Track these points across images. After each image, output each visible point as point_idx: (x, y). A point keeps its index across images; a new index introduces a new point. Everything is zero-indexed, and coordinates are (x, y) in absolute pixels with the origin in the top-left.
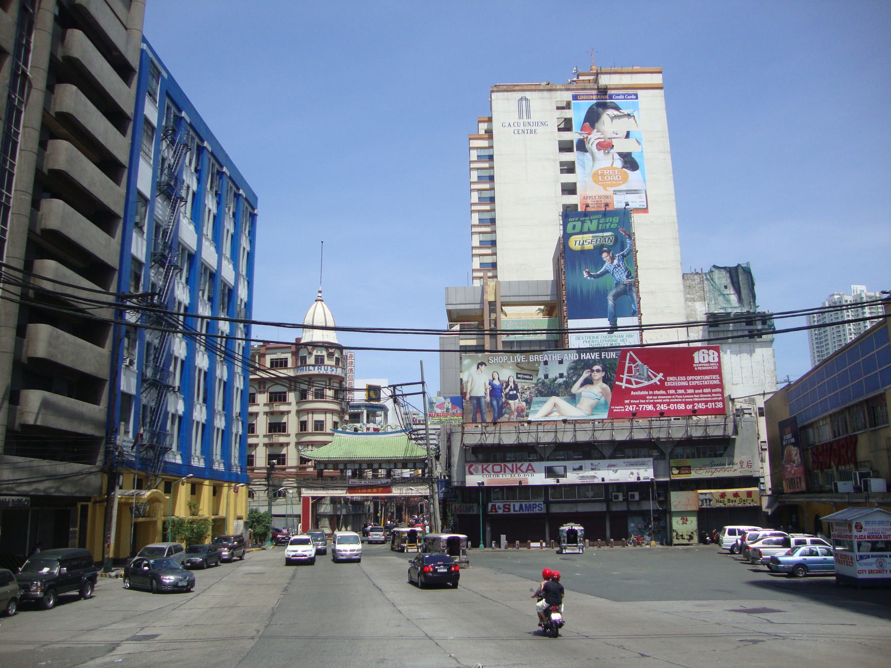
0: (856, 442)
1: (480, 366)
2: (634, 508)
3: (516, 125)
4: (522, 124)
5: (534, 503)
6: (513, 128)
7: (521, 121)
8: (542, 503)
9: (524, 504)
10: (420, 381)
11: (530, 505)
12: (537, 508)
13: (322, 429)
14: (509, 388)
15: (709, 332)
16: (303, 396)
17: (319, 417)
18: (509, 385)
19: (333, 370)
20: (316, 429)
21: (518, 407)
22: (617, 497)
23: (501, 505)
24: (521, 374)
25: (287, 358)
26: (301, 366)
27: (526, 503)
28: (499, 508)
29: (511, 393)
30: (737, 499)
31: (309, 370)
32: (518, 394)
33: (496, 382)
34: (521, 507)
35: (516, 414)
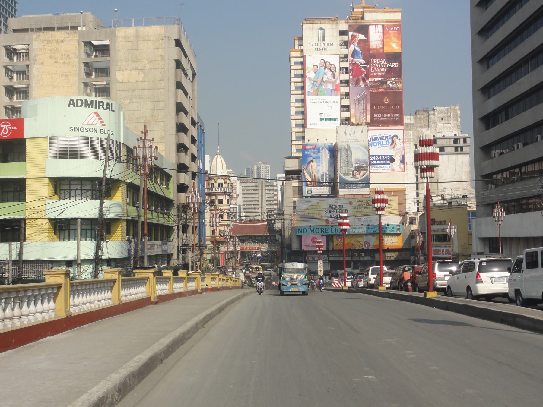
2: (361, 259)
3: (316, 45)
4: (320, 45)
6: (315, 47)
7: (320, 42)
23: (311, 257)
28: (310, 258)
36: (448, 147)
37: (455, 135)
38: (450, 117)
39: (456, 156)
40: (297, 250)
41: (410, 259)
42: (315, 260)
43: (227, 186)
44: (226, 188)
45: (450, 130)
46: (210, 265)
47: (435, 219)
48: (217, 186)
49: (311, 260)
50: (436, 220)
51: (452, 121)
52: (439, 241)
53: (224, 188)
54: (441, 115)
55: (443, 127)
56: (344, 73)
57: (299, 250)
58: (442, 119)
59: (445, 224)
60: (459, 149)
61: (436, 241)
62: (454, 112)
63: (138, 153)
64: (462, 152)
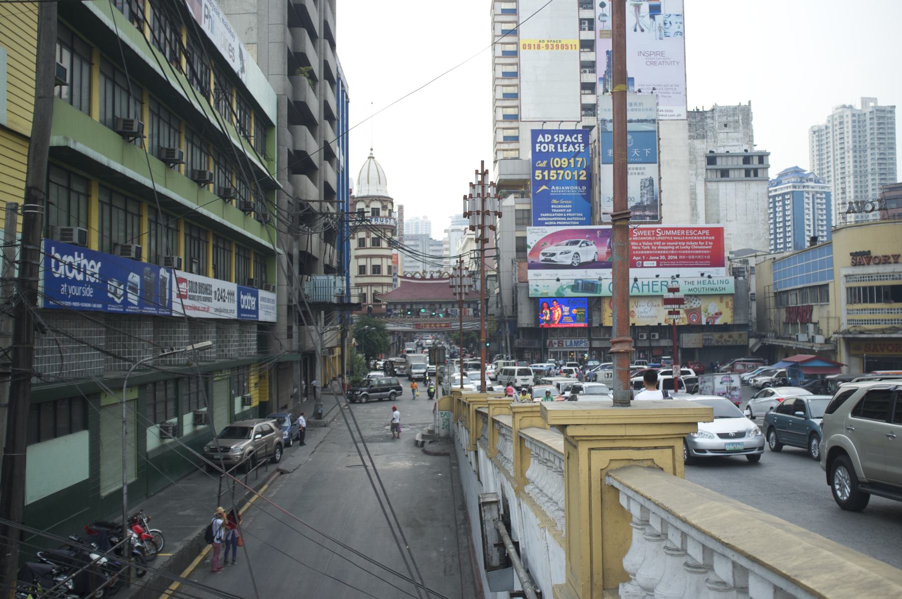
0: (812, 310)
2: (654, 344)
10: (495, 246)
13: (379, 272)
15: (707, 169)
17: (377, 262)
20: (374, 273)
22: (642, 336)
23: (556, 341)
30: (731, 340)
34: (571, 342)
36: (734, 169)
37: (746, 151)
38: (737, 122)
39: (747, 183)
40: (530, 326)
41: (748, 346)
42: (564, 346)
44: (386, 218)
45: (737, 144)
46: (360, 356)
47: (869, 252)
50: (873, 254)
51: (741, 128)
52: (879, 301)
53: (383, 217)
54: (724, 119)
55: (727, 139)
56: (587, 28)
57: (533, 326)
58: (726, 126)
59: (896, 262)
60: (752, 173)
61: (872, 301)
62: (743, 115)
64: (756, 178)
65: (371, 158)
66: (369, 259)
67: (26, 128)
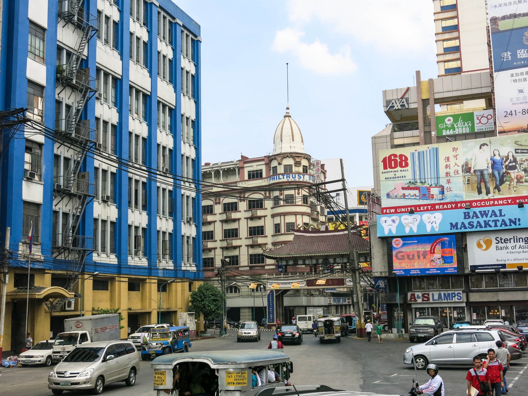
1: (482, 147)
5: (453, 292)
8: (461, 292)
9: (442, 293)
11: (449, 294)
12: (456, 297)
14: (509, 161)
16: (276, 200)
18: (508, 159)
19: (301, 178)
21: (517, 176)
23: (420, 294)
24: (519, 149)
25: (262, 170)
26: (272, 176)
27: (446, 292)
28: (419, 297)
29: (511, 164)
31: (279, 179)
32: (517, 165)
33: (497, 158)
34: (440, 295)
35: (516, 180)
42: (431, 301)
43: (301, 169)
48: (282, 171)
49: (420, 301)
63: (255, 268)
65: (287, 116)
66: (282, 217)
67: (60, 144)
